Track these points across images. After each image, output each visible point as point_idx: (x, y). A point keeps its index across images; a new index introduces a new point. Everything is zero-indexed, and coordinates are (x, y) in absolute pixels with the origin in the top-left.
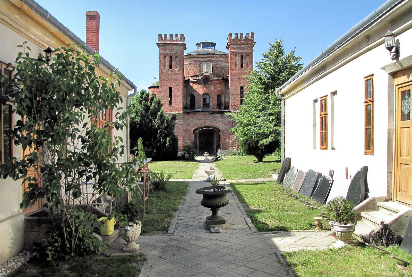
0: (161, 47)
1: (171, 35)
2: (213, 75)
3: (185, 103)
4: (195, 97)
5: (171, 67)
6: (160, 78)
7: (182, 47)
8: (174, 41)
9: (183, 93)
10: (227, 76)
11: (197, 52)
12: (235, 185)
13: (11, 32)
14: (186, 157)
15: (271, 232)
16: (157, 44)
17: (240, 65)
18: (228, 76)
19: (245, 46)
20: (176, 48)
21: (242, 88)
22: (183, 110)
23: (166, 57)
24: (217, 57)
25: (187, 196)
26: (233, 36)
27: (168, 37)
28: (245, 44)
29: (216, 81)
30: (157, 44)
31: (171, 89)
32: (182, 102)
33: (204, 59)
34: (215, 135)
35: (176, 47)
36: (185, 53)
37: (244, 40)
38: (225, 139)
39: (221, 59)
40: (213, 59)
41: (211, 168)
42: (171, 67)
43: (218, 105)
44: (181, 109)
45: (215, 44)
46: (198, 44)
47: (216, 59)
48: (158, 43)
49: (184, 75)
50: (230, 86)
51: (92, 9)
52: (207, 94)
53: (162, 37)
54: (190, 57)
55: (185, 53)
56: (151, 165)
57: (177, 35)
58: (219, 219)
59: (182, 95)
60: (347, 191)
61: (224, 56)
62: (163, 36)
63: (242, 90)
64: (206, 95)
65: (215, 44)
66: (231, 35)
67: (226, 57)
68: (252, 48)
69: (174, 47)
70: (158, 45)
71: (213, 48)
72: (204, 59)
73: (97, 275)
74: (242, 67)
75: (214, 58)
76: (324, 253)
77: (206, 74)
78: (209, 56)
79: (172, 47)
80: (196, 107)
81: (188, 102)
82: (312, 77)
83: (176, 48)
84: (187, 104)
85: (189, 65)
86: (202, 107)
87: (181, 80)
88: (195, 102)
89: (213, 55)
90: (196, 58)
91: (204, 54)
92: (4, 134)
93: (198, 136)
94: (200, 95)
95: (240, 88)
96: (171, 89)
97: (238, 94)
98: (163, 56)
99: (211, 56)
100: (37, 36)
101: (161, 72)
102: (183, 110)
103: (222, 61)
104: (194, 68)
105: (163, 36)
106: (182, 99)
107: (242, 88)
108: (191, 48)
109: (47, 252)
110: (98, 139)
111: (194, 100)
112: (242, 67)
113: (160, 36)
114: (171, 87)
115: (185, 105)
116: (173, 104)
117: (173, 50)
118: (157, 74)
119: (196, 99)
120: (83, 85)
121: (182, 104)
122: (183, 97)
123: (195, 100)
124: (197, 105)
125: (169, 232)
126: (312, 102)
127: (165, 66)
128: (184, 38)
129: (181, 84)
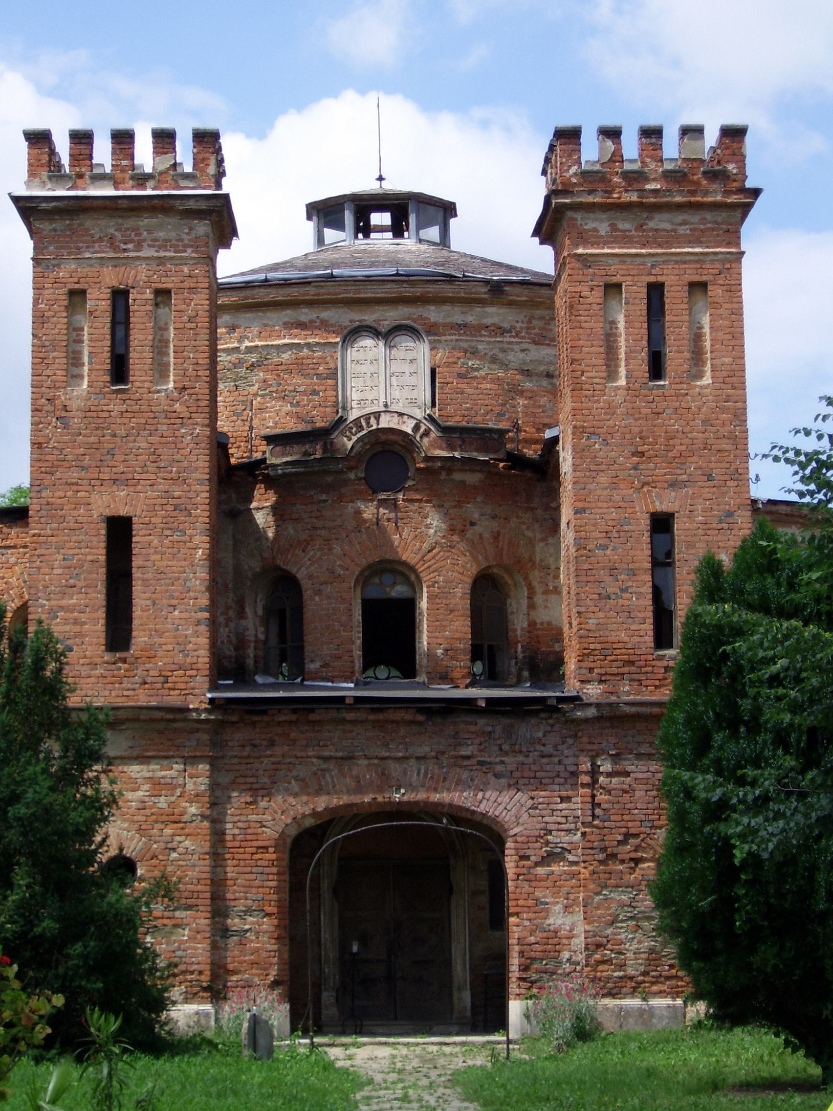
0: (45, 226)
1: (123, 140)
2: (435, 433)
3: (223, 632)
4: (307, 594)
5: (119, 370)
6: (37, 445)
7: (202, 228)
8: (142, 179)
9: (214, 563)
10: (548, 434)
11: (316, 266)
12: (816, 1071)
13: (292, 426)
14: (751, 877)
15: (326, 297)
16: (16, 200)
17: (644, 355)
18: (555, 440)
19: (680, 217)
20: (161, 234)
21: (662, 524)
22: (214, 687)
23: (83, 293)
24: (470, 301)
25: (604, 1022)
26: (591, 151)
27: (103, 153)
28: (680, 207)
29: (473, 478)
30: (16, 200)
31: (119, 531)
32: (203, 629)
33: (369, 317)
34: (466, 881)
35: (161, 226)
36: (232, 264)
37: (668, 175)
38: (540, 908)
39: (494, 315)
40: (433, 314)
41: (162, 295)
42: (119, 370)
43: (476, 653)
44: (201, 682)
45: (448, 210)
46: (325, 212)
47: (457, 315)
48: (23, 192)
49: (223, 425)
50: (566, 514)
51: (78, 126)
52: (394, 572)
53: (52, 152)
54: (266, 295)
55: (232, 264)
56: (400, 400)
57: (164, 139)
58: (586, 701)
59: (203, 574)
60: (348, 192)
61: (522, 294)
62: (63, 147)
63: (662, 537)
64: (387, 578)
65: (448, 210)
66: (568, 137)
67: (533, 304)
68: (733, 236)
69: (146, 222)
70: (28, 208)
71: (433, 233)
72: (369, 317)
73: (212, 1071)
74: (656, 369)
75: (447, 308)
76: (212, 954)
77: (386, 422)
78: (407, 291)
79: (131, 222)
80: (312, 667)
81: (253, 625)
82: (344, 1033)
83: (161, 234)
84: (241, 644)
85: (253, 358)
86: (358, 664)
87: (200, 465)
88: (307, 628)
89: (431, 289)
90: (310, 304)
91: (369, 280)
92: (145, 189)
93: (325, 886)
94: (739, 476)
95: (645, 523)
96: (119, 531)
97: (633, 573)
98: (59, 303)
99: (418, 291)
100: (352, 283)
101: (46, 407)
102: (214, 687)
103: (502, 331)
104: (297, 380)
105: (63, 147)
106: (204, 601)
107: (662, 524)
108: (269, 236)
109: (734, 851)
110: (318, 1085)
111: (299, 609)
112: (656, 369)
113: (39, 139)
114: (123, 511)
115: (229, 651)
116: (140, 638)
117: (139, 247)
118: (219, 256)
119: (314, 605)
120: (365, 515)
121: (204, 641)
122: (215, 587)
123: (308, 615)
124: (318, 646)
125: (415, 422)
126: (547, 137)
127: (75, 360)
128: (220, 162)
129: (199, 494)
